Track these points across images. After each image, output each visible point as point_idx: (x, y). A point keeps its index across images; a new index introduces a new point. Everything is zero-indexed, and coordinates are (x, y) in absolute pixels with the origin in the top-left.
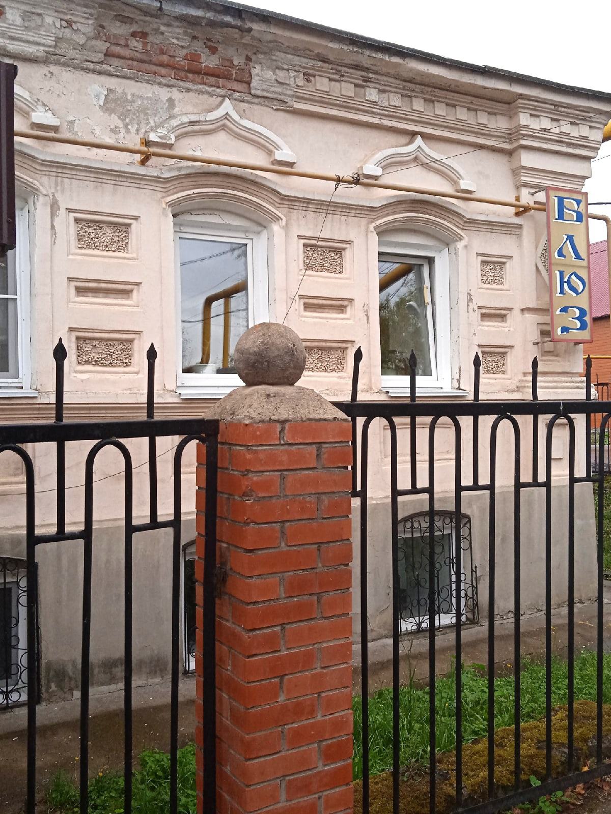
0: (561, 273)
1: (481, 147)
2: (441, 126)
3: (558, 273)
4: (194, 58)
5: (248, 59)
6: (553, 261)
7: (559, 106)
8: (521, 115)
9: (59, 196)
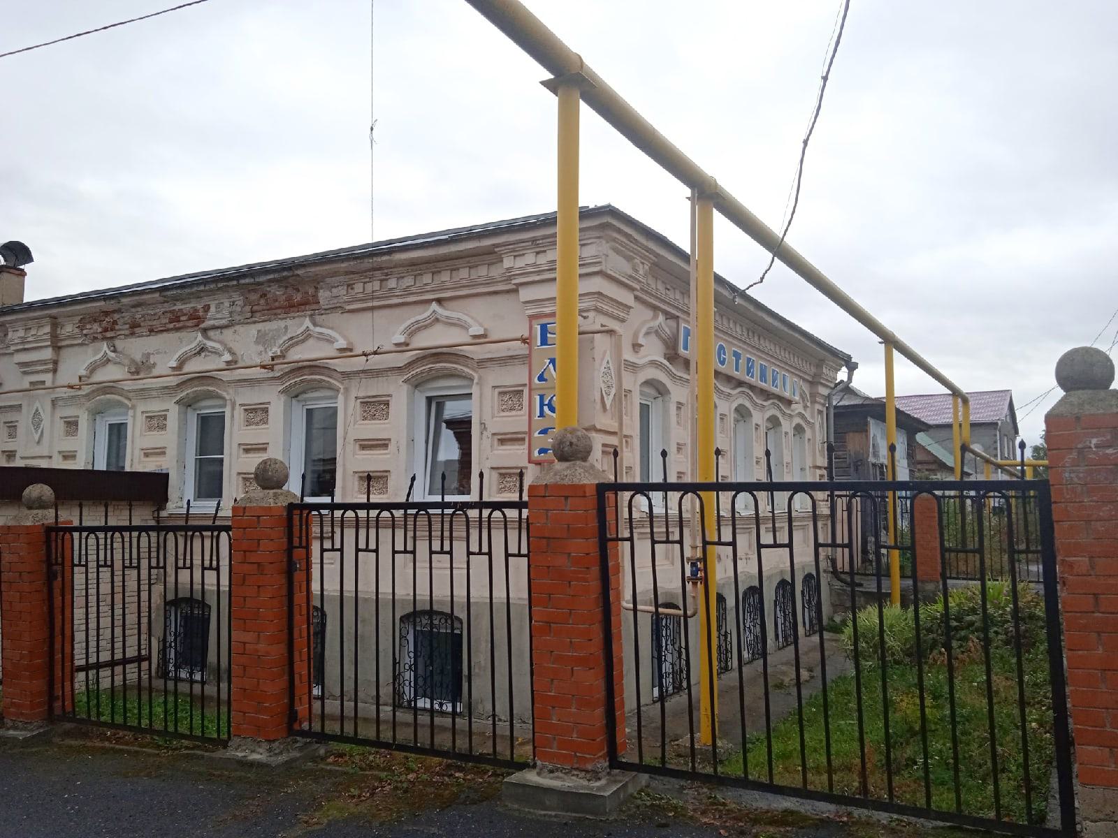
0: (542, 397)
1: (496, 293)
2: (468, 286)
3: (538, 398)
4: (289, 299)
5: (316, 288)
6: (533, 386)
7: (536, 240)
8: (505, 260)
9: (236, 399)
